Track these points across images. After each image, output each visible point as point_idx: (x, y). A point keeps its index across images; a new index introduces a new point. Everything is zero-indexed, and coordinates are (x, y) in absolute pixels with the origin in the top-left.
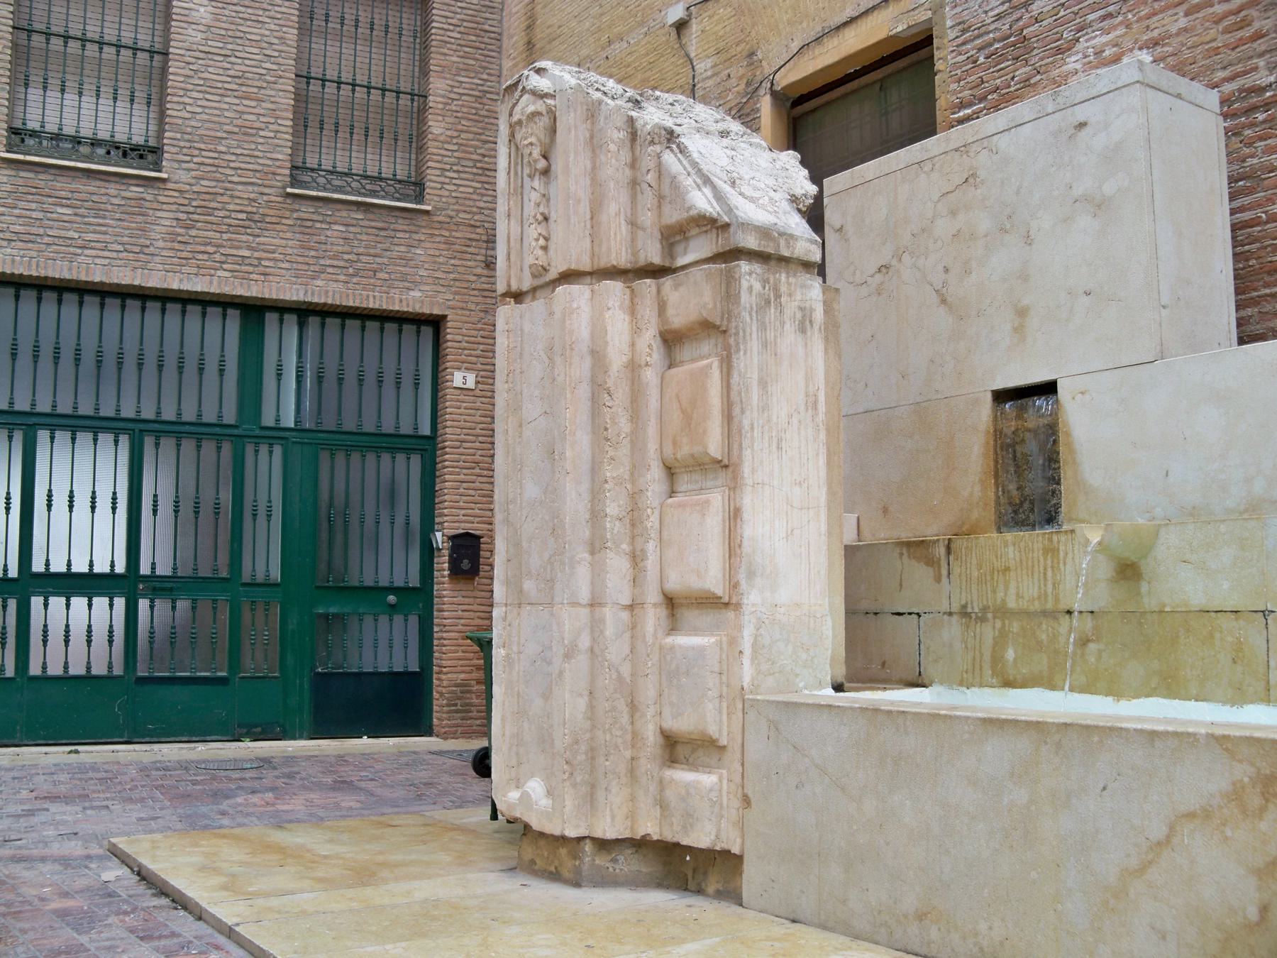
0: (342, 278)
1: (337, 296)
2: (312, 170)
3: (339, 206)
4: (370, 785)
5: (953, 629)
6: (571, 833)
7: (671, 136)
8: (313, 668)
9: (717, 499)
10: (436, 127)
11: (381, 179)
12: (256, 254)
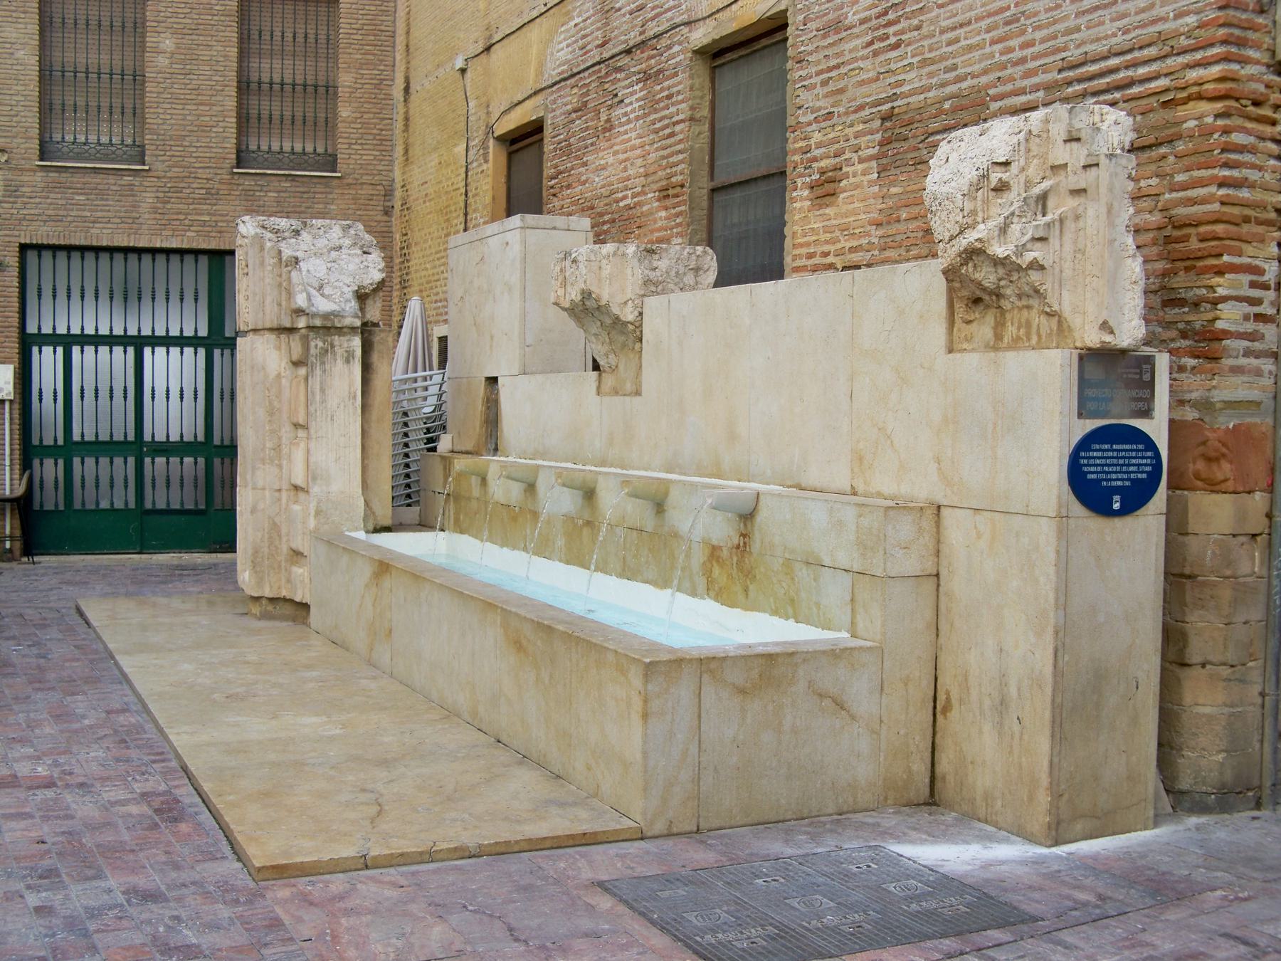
7: (297, 260)
12: (214, 218)
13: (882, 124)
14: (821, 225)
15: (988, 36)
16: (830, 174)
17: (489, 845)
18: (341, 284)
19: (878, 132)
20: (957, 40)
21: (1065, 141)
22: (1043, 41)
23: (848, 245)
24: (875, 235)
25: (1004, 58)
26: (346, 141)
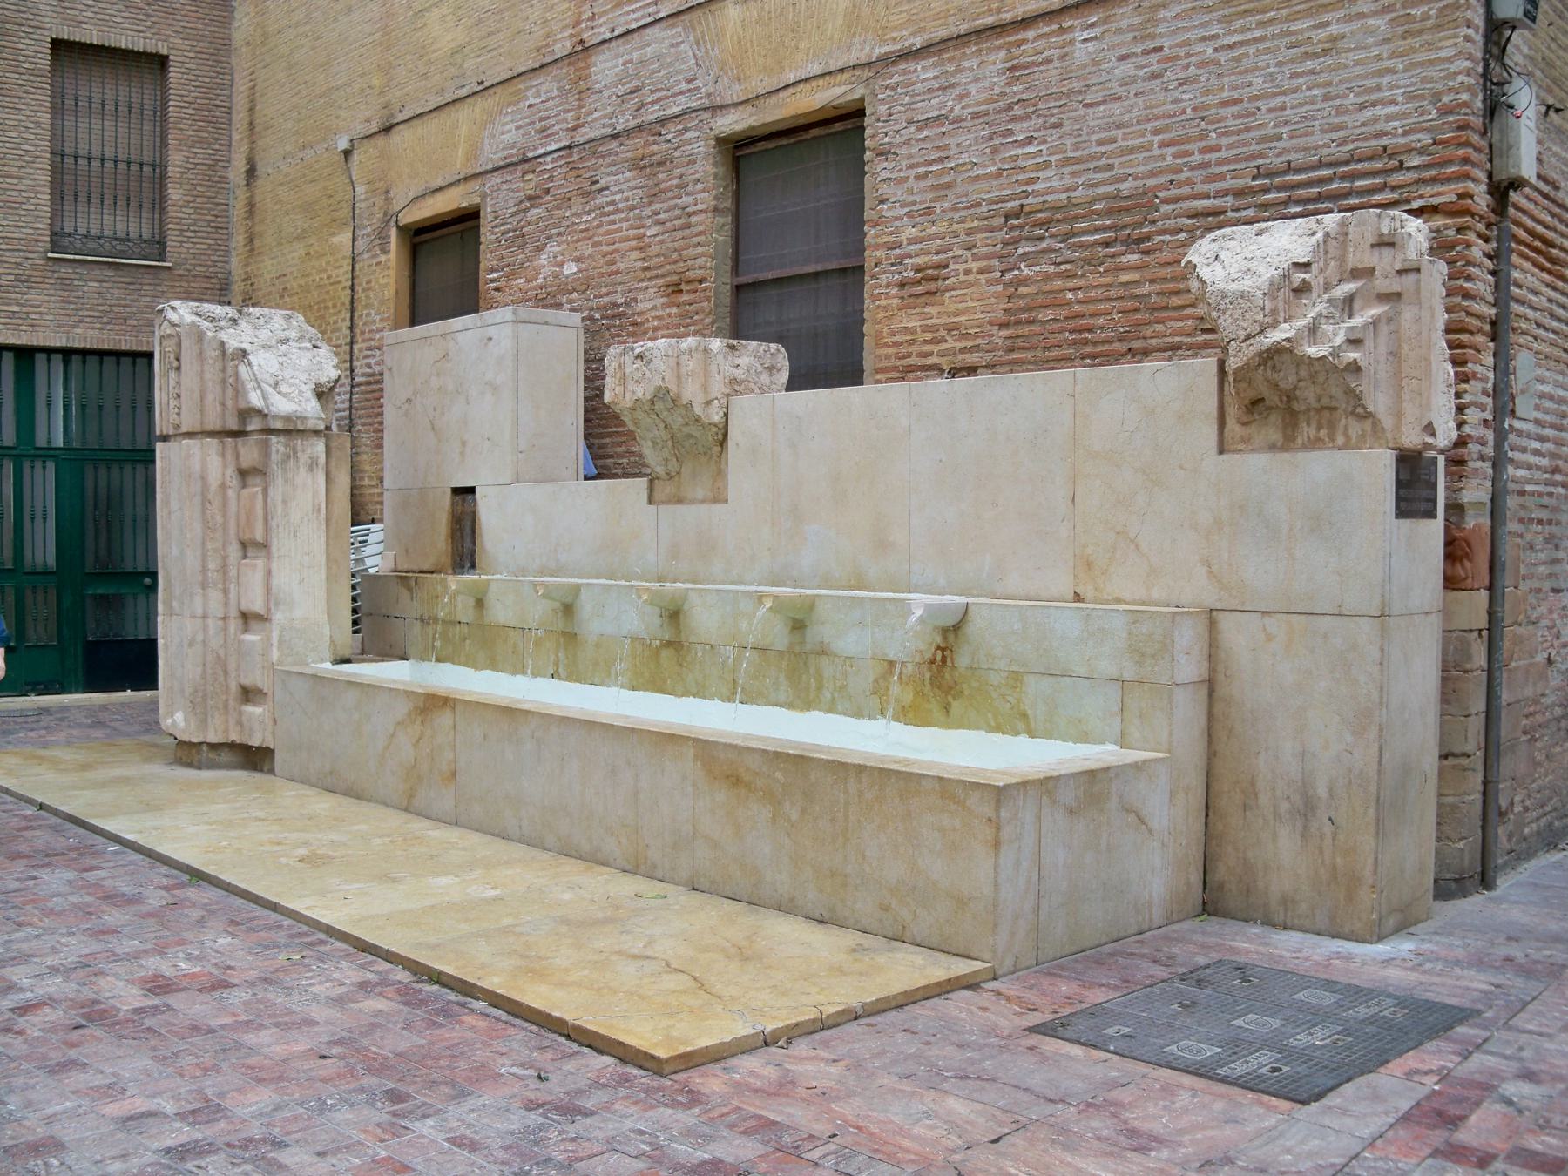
0: (98, 326)
1: (95, 341)
2: (70, 235)
3: (94, 266)
4: (117, 724)
5: (417, 628)
6: (195, 740)
7: (244, 354)
8: (86, 637)
9: (260, 563)
10: (175, 193)
11: (129, 240)
12: (24, 309)
13: (1006, 222)
14: (918, 324)
15: (1156, 139)
16: (930, 271)
17: (872, 1002)
18: (297, 381)
19: (1001, 230)
20: (1113, 141)
21: (1373, 246)
22: (1230, 147)
23: (959, 345)
24: (999, 336)
25: (1179, 161)
26: (178, 227)
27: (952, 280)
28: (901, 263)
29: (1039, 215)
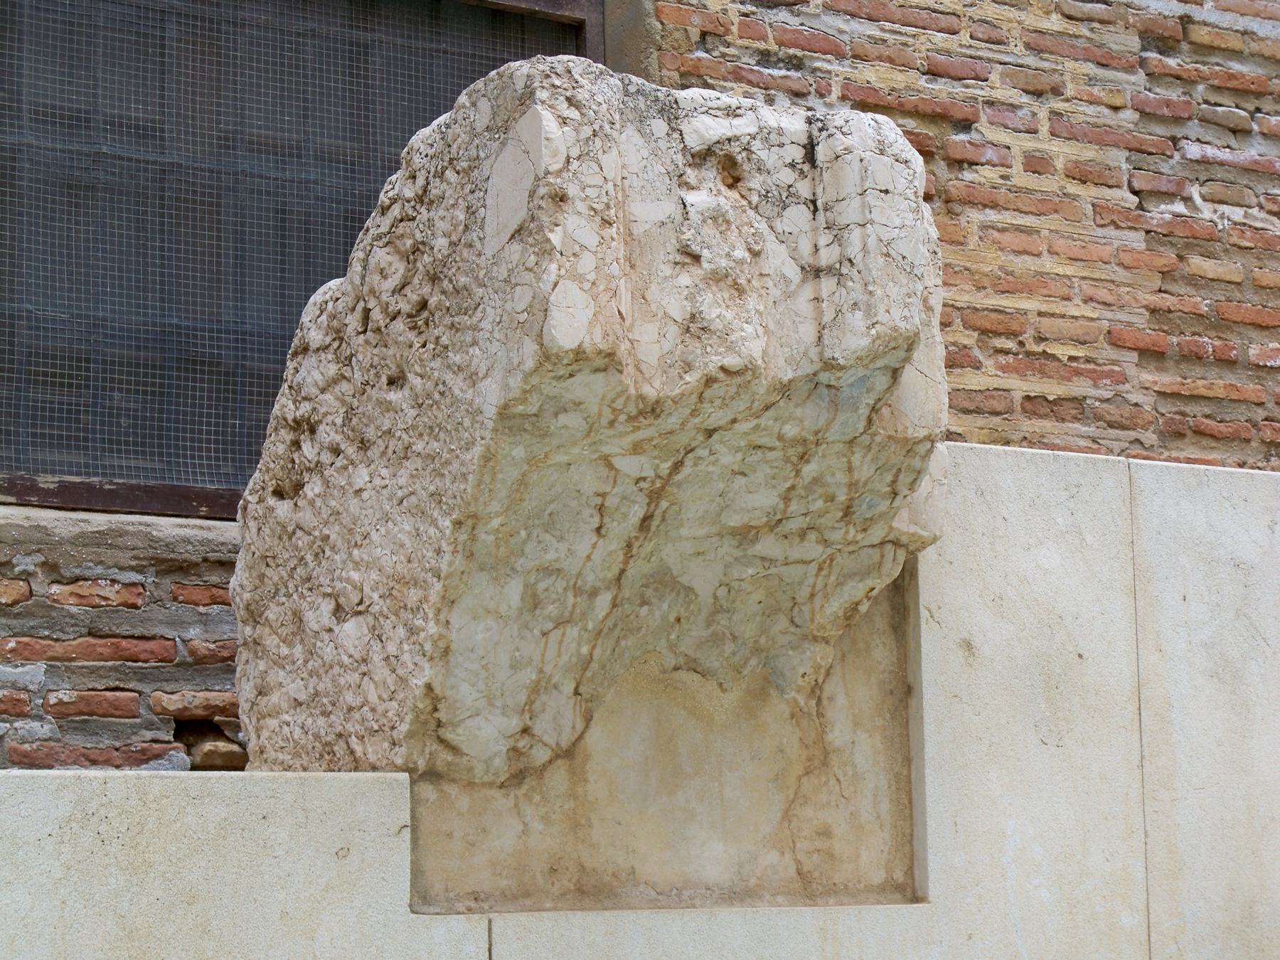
23: (1020, 386)
27: (987, 174)
28: (796, 64)
29: (1236, 67)
